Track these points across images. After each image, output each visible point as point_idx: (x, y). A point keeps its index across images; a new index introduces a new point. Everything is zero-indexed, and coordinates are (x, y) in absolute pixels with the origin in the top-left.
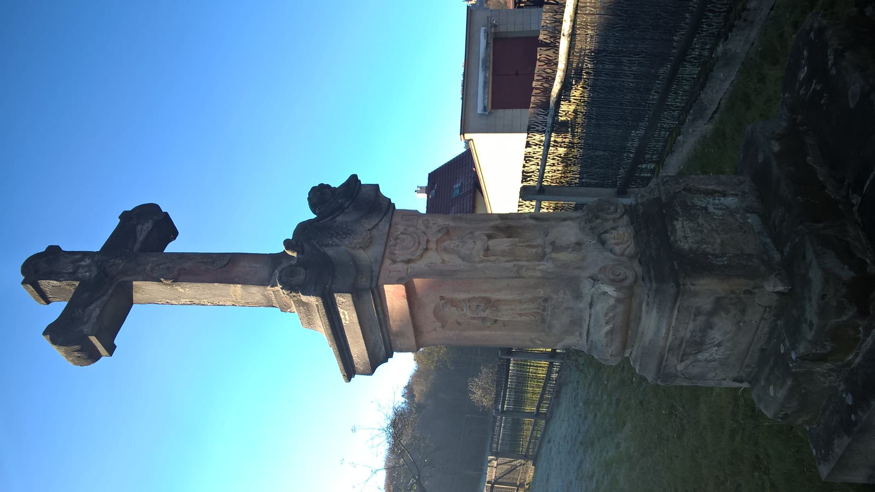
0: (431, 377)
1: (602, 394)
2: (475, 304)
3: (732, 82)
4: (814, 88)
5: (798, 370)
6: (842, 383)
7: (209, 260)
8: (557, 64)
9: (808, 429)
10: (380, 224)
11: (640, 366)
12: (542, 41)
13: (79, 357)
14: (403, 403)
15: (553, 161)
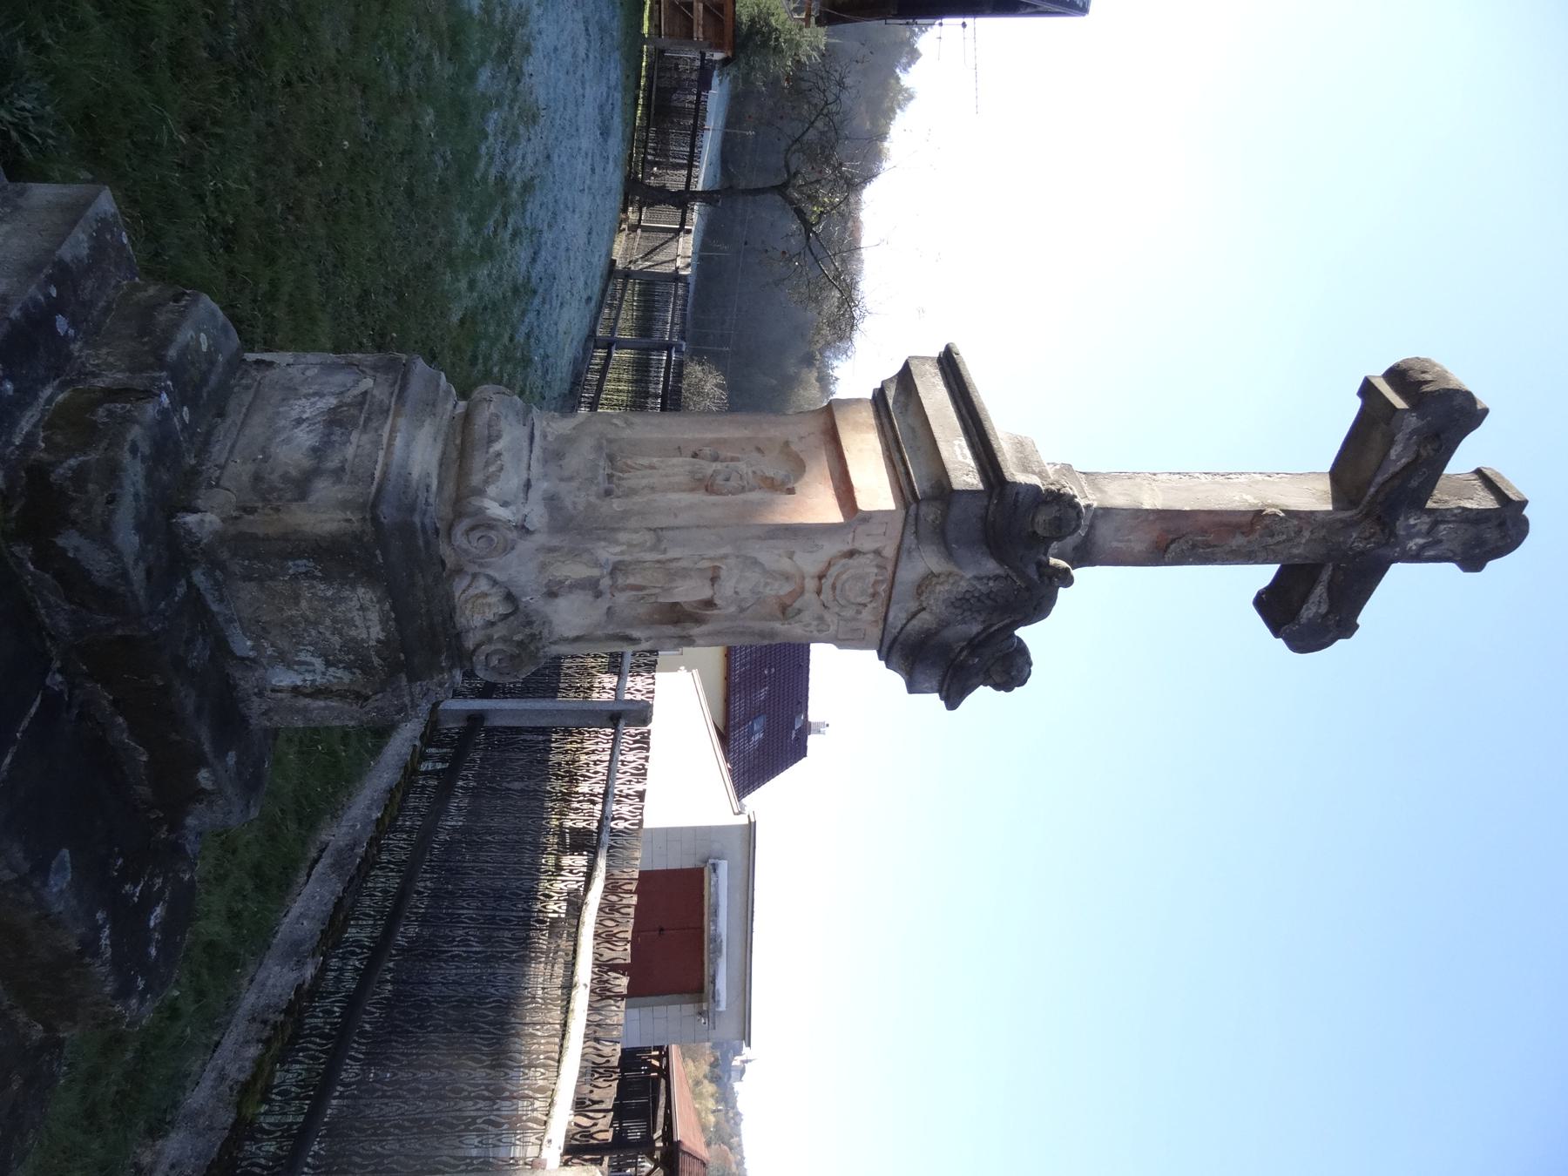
1: (502, 377)
2: (733, 483)
4: (136, 887)
5: (157, 374)
6: (76, 354)
7: (1201, 550)
8: (595, 935)
10: (904, 622)
12: (624, 974)
13: (1423, 372)
15: (598, 768)
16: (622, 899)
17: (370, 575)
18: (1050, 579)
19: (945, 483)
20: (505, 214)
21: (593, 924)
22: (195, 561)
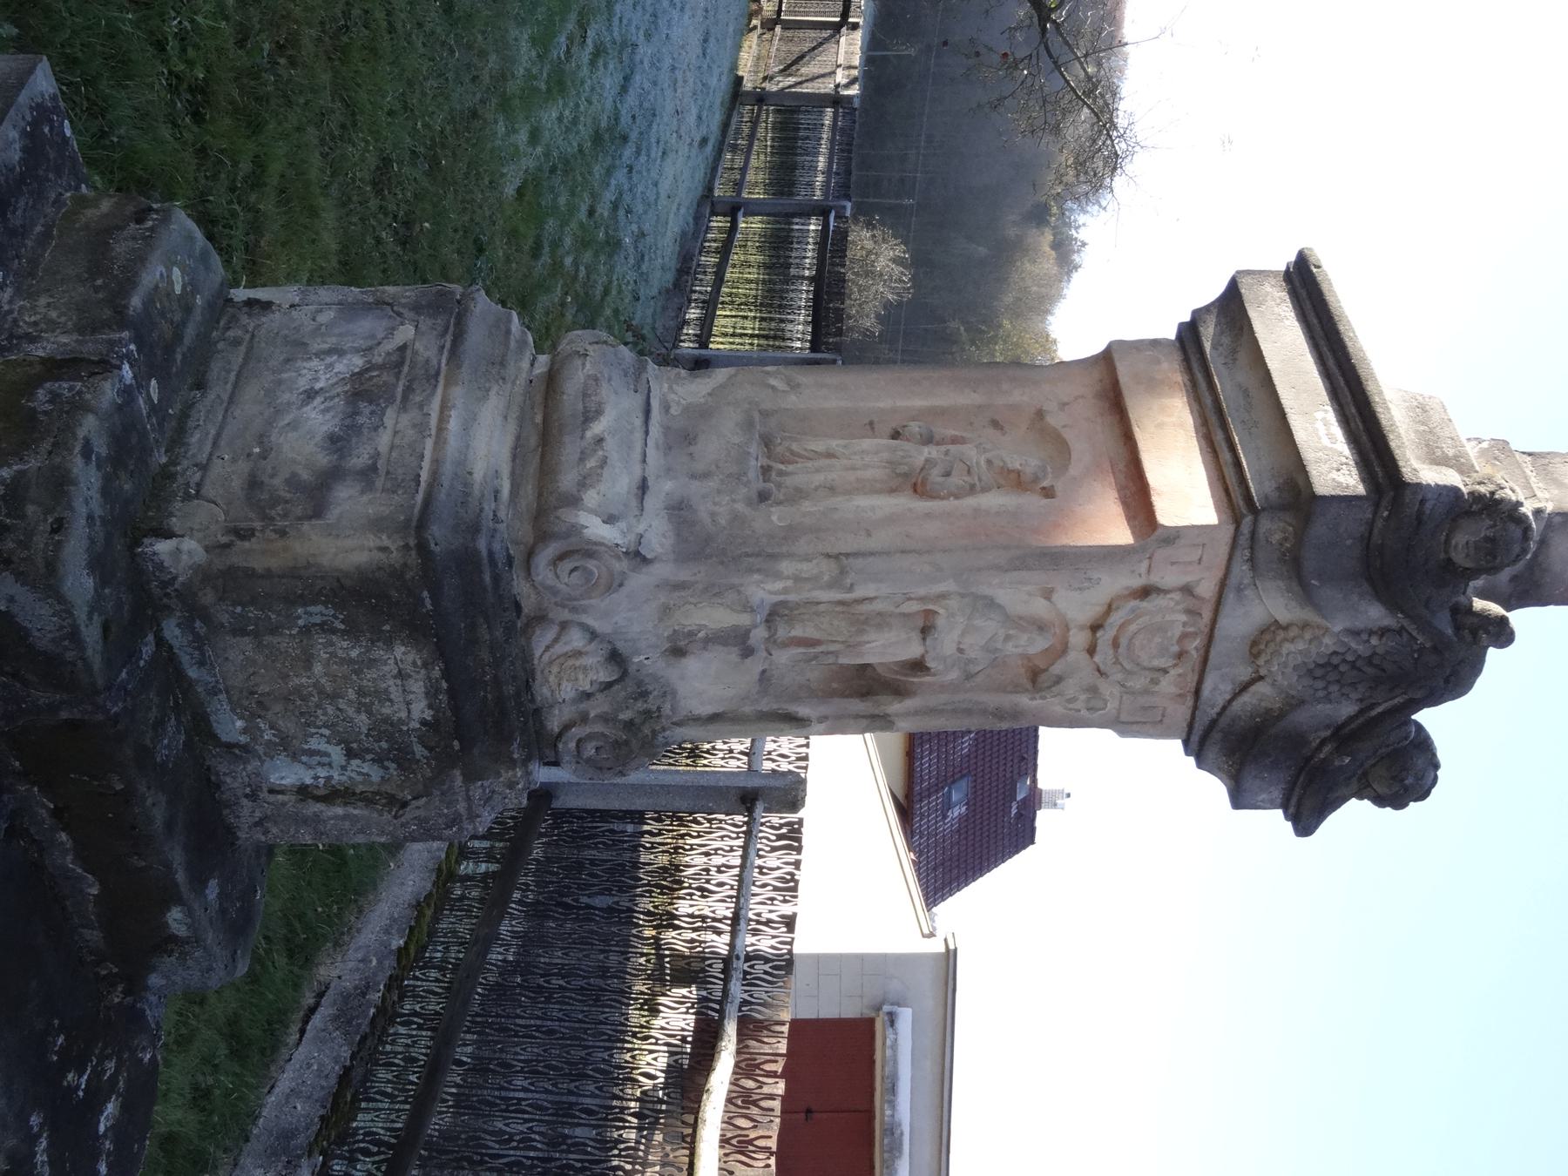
0: (1009, 299)
1: (577, 270)
2: (957, 480)
3: (272, 1087)
4: (80, 1077)
8: (722, 1141)
9: (83, 186)
10: (1228, 697)
11: (508, 332)
14: (1084, 225)
15: (723, 878)
16: (761, 1085)
17: (415, 628)
18: (1474, 633)
19: (1301, 482)
20: (583, 26)
21: (719, 1125)
22: (168, 607)
